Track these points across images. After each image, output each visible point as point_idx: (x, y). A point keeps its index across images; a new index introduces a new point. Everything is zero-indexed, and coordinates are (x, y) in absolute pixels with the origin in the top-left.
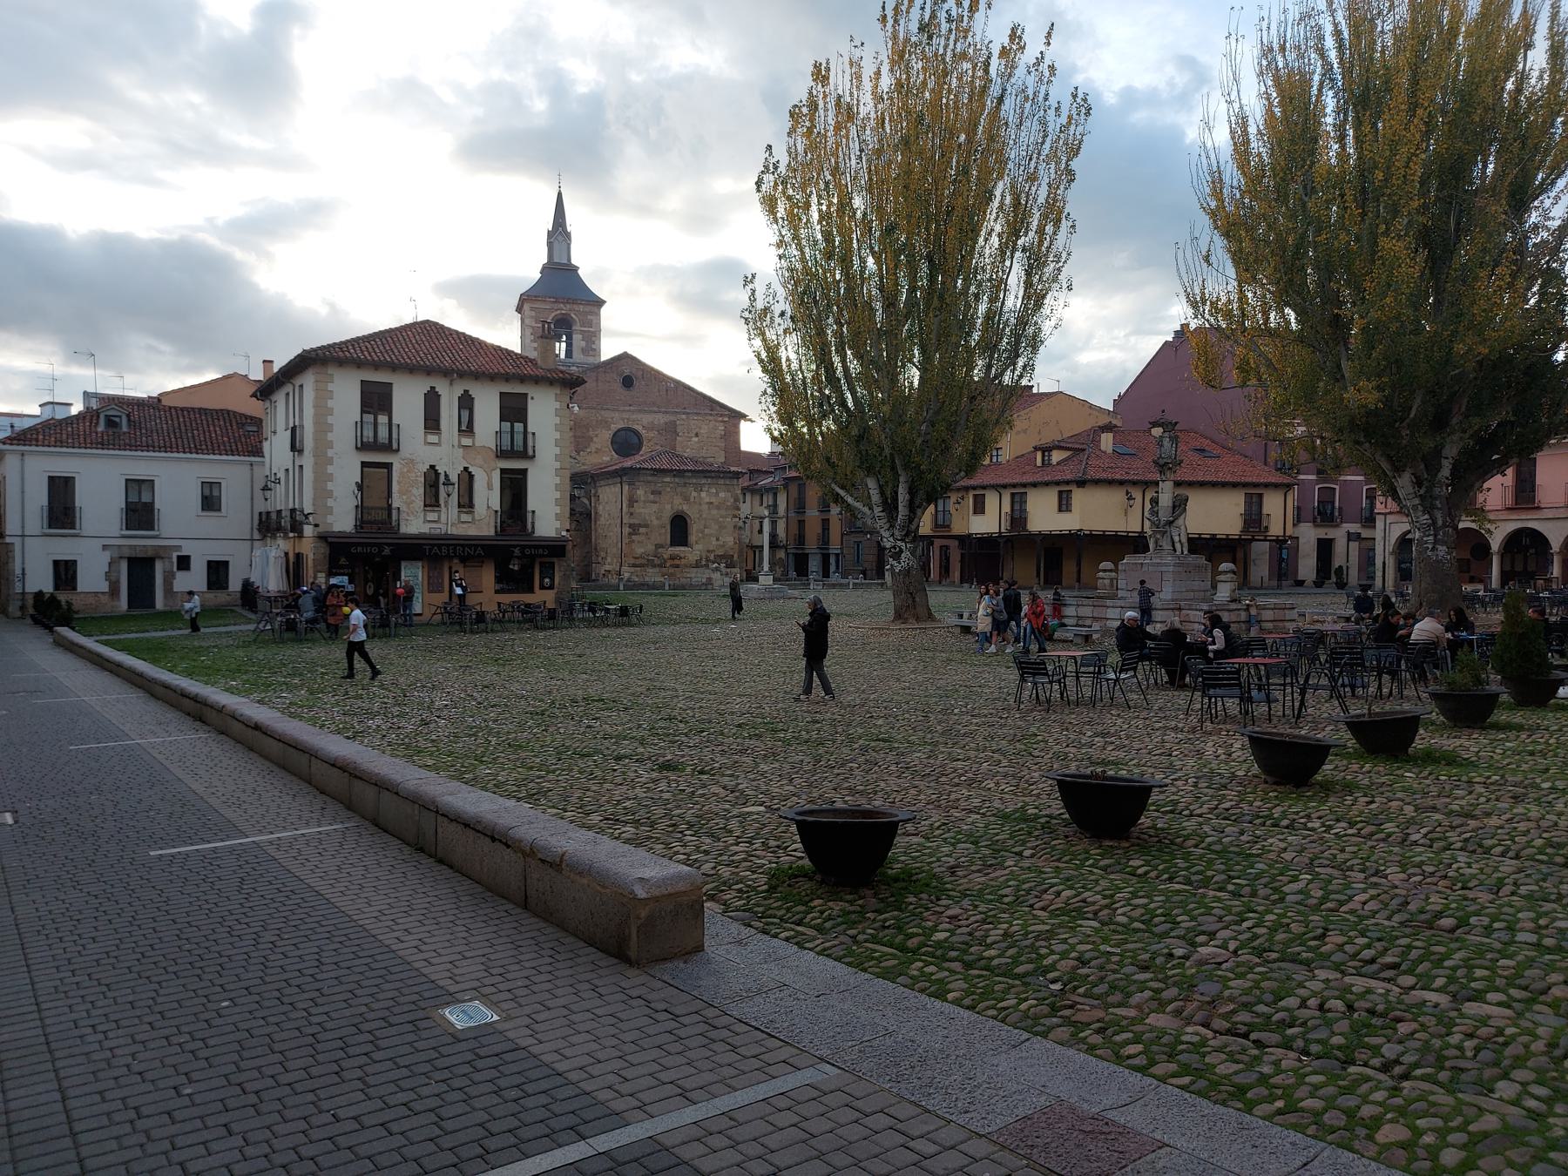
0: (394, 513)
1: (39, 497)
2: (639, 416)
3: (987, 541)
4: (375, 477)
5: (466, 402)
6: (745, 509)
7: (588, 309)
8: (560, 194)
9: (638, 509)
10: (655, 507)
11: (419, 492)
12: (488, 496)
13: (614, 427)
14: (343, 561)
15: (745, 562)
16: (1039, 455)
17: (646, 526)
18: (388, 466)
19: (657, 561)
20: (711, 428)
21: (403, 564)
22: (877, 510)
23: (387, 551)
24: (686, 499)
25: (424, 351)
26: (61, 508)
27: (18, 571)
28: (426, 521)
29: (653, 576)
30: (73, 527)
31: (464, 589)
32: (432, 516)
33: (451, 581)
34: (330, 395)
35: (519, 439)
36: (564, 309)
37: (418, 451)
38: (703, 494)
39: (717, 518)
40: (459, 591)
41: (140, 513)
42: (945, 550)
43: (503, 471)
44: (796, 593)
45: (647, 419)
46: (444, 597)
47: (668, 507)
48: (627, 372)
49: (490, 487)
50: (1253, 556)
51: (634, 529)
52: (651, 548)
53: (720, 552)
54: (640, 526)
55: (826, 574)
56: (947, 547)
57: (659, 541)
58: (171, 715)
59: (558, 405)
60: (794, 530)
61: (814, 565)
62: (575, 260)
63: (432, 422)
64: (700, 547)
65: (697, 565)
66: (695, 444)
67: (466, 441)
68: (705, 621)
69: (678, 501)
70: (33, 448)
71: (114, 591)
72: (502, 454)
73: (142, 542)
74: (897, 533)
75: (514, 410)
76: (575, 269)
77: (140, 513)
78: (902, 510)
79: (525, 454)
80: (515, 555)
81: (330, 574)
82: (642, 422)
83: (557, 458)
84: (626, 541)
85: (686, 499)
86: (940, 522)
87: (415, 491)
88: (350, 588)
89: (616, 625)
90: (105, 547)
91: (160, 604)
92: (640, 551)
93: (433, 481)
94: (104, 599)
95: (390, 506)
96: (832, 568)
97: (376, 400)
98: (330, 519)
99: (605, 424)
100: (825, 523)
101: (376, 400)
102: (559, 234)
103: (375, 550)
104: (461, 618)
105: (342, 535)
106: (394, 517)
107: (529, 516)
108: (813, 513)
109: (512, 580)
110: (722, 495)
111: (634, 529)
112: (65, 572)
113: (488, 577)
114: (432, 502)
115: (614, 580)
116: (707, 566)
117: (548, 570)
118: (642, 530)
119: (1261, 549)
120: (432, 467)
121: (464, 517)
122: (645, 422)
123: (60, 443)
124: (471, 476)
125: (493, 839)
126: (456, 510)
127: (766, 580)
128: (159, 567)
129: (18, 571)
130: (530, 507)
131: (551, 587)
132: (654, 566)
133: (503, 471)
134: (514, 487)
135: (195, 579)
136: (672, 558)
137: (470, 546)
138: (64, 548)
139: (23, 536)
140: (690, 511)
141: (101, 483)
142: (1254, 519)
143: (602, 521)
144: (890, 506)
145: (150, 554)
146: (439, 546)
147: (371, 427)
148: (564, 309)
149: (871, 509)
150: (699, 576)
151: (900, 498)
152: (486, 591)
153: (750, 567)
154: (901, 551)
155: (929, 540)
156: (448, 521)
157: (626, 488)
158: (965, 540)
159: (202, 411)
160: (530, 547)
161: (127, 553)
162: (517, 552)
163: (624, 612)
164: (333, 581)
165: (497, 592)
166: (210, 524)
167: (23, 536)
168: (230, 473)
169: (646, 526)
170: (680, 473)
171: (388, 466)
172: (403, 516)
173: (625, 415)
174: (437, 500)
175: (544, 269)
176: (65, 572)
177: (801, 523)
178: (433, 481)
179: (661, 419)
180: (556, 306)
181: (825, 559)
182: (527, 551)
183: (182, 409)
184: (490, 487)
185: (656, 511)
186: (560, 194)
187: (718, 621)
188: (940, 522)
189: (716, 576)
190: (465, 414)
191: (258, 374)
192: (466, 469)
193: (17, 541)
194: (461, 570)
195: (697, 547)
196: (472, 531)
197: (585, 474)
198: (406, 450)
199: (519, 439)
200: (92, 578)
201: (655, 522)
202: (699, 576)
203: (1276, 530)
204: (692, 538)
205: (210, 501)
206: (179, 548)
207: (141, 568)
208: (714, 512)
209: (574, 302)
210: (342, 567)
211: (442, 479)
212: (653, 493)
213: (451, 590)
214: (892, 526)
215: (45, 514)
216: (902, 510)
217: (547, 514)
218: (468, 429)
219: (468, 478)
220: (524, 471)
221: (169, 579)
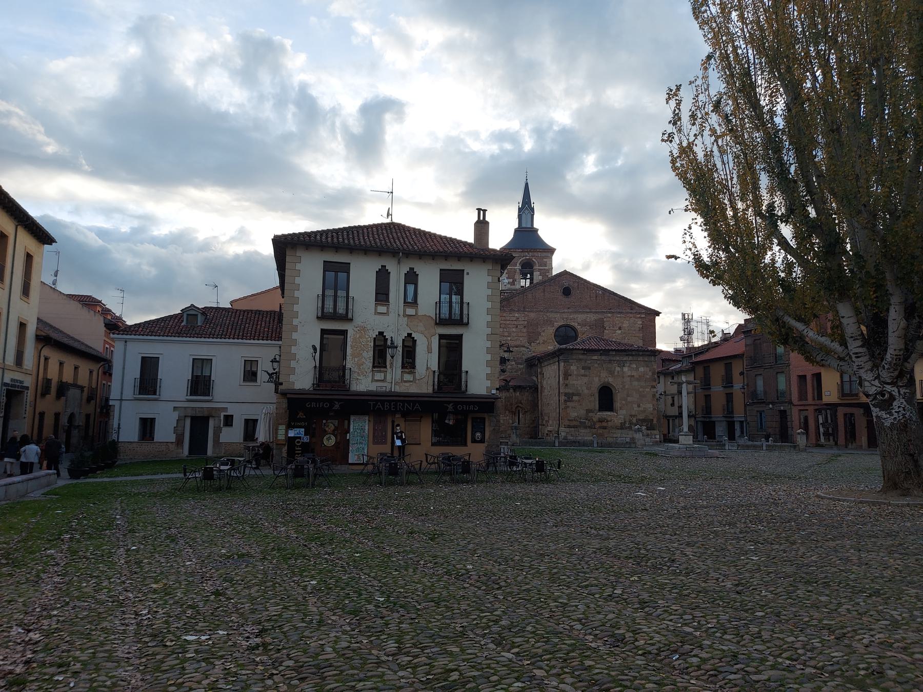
0: (347, 372)
1: (134, 371)
2: (575, 316)
4: (332, 342)
5: (411, 278)
6: (660, 388)
7: (544, 254)
8: (527, 185)
9: (572, 381)
10: (585, 380)
11: (368, 355)
12: (428, 358)
13: (557, 325)
14: (301, 415)
15: (665, 427)
17: (579, 395)
18: (344, 333)
19: (588, 423)
20: (630, 324)
21: (352, 418)
22: (854, 346)
23: (337, 406)
24: (611, 373)
25: (394, 244)
26: (148, 381)
27: (115, 426)
28: (373, 380)
29: (585, 435)
30: (155, 393)
31: (403, 441)
32: (380, 376)
33: (393, 433)
35: (456, 308)
36: (528, 256)
37: (368, 319)
38: (626, 369)
39: (635, 390)
40: (398, 443)
41: (200, 384)
42: (849, 418)
43: (441, 337)
44: (716, 452)
45: (580, 317)
46: (386, 449)
47: (596, 379)
48: (566, 285)
49: (430, 351)
51: (569, 397)
52: (582, 412)
53: (641, 417)
54: (573, 394)
55: (732, 437)
56: (852, 415)
59: (490, 279)
60: (702, 402)
61: (721, 430)
62: (535, 226)
63: (382, 295)
64: (624, 412)
65: (622, 427)
66: (620, 332)
67: (410, 311)
68: (628, 480)
69: (604, 374)
70: (133, 337)
71: (179, 441)
72: (441, 322)
73: (201, 404)
74: (885, 375)
75: (453, 282)
76: (536, 230)
77: (200, 384)
78: (894, 343)
79: (461, 322)
80: (451, 410)
81: (290, 427)
82: (578, 320)
83: (488, 324)
84: (562, 406)
85: (611, 373)
86: (847, 390)
87: (365, 354)
88: (306, 439)
89: (534, 481)
90: (175, 408)
91: (210, 452)
92: (574, 414)
93: (381, 348)
94: (172, 447)
95: (344, 367)
96: (738, 433)
97: (336, 273)
98: (292, 378)
99: (550, 322)
100: (729, 397)
101: (336, 273)
103: (326, 405)
104: (391, 471)
105: (301, 392)
106: (347, 377)
107: (463, 375)
108: (717, 389)
109: (449, 434)
110: (641, 369)
111: (569, 397)
112: (147, 426)
113: (425, 430)
115: (550, 439)
116: (630, 428)
117: (479, 425)
118: (575, 398)
120: (381, 333)
121: (407, 377)
122: (579, 320)
123: (152, 333)
124: (414, 341)
126: (399, 371)
127: (686, 440)
128: (211, 423)
129: (115, 426)
130: (464, 369)
131: (482, 441)
132: (586, 427)
133: (441, 337)
134: (452, 349)
135: (233, 435)
136: (601, 421)
137: (409, 402)
138: (147, 409)
139: (121, 400)
141: (176, 361)
143: (546, 392)
144: (875, 341)
145: (206, 414)
146: (383, 402)
147: (332, 299)
148: (528, 256)
149: (844, 343)
150: (624, 436)
151: (892, 326)
152: (422, 444)
153: (666, 432)
154: (892, 398)
155: (833, 407)
156: (393, 380)
157: (562, 364)
159: (259, 312)
160: (462, 403)
161: (190, 413)
162: (450, 407)
163: (540, 467)
164: (291, 434)
165: (433, 445)
166: (249, 391)
167: (121, 400)
168: (262, 353)
170: (606, 352)
171: (344, 333)
172: (355, 376)
173: (565, 316)
174: (385, 363)
175: (516, 231)
176: (147, 426)
177: (708, 397)
178: (381, 349)
179: (592, 317)
180: (522, 254)
181: (731, 426)
182: (460, 407)
183: (244, 311)
184: (430, 351)
185: (586, 381)
186: (527, 185)
187: (642, 480)
188: (847, 390)
189: (638, 436)
190: (411, 288)
192: (409, 335)
193: (117, 404)
194: (402, 424)
195: (621, 412)
196: (413, 389)
197: (534, 358)
198: (359, 319)
199: (456, 308)
200: (164, 433)
201: (586, 391)
202: (624, 436)
204: (617, 405)
205: (250, 375)
206: (225, 409)
207: (199, 423)
208: (636, 383)
209: (535, 250)
210: (301, 420)
211: (389, 343)
212: (583, 368)
213: (393, 442)
214: (875, 366)
215: (138, 384)
217: (479, 376)
220: (460, 337)
221: (218, 431)
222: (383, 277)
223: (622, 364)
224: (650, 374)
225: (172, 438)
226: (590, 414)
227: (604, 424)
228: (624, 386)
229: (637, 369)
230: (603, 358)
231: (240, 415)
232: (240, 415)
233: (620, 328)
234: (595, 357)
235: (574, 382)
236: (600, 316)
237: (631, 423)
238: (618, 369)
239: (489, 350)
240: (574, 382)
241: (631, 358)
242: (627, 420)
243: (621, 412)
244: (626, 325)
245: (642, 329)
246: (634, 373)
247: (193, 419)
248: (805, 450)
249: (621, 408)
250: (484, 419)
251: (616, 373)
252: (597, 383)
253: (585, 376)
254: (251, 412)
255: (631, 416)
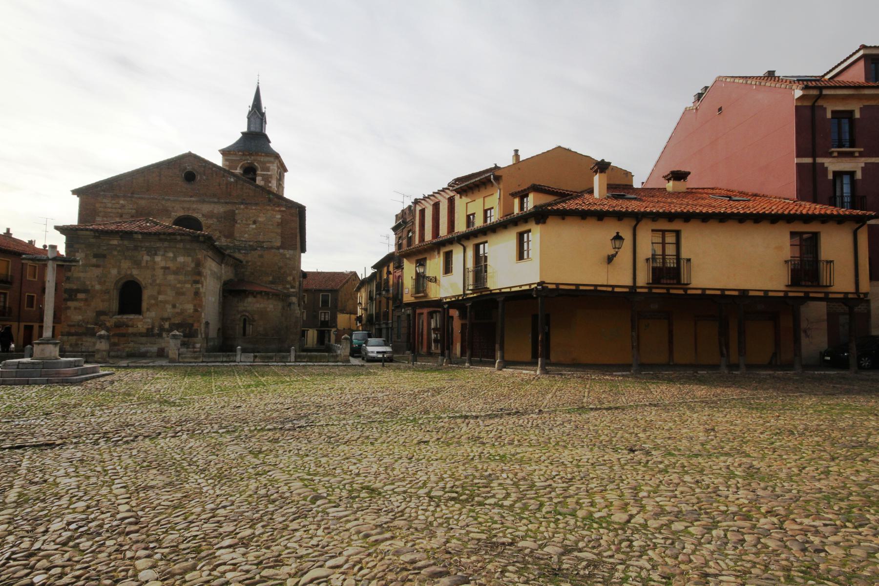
7: (267, 159)
10: (97, 272)
16: (517, 201)
17: (86, 291)
24: (137, 264)
38: (158, 259)
45: (206, 208)
50: (804, 325)
52: (91, 314)
53: (177, 321)
57: (102, 306)
58: (617, 377)
64: (153, 314)
102: (257, 113)
110: (181, 259)
118: (81, 296)
119: (815, 311)
142: (807, 269)
169: (86, 291)
179: (220, 209)
180: (244, 158)
201: (98, 287)
203: (841, 281)
208: (171, 278)
212: (96, 256)
223: (153, 252)
224: (193, 265)
226: (102, 318)
227: (123, 330)
228: (155, 281)
229: (175, 258)
230: (126, 243)
233: (255, 222)
234: (115, 242)
235: (82, 275)
236: (229, 207)
237: (162, 329)
238: (146, 258)
240: (82, 275)
241: (166, 244)
242: (157, 324)
243: (148, 314)
246: (170, 264)
249: (148, 310)
250: (380, 337)
251: (144, 264)
253: (98, 266)
255: (163, 319)
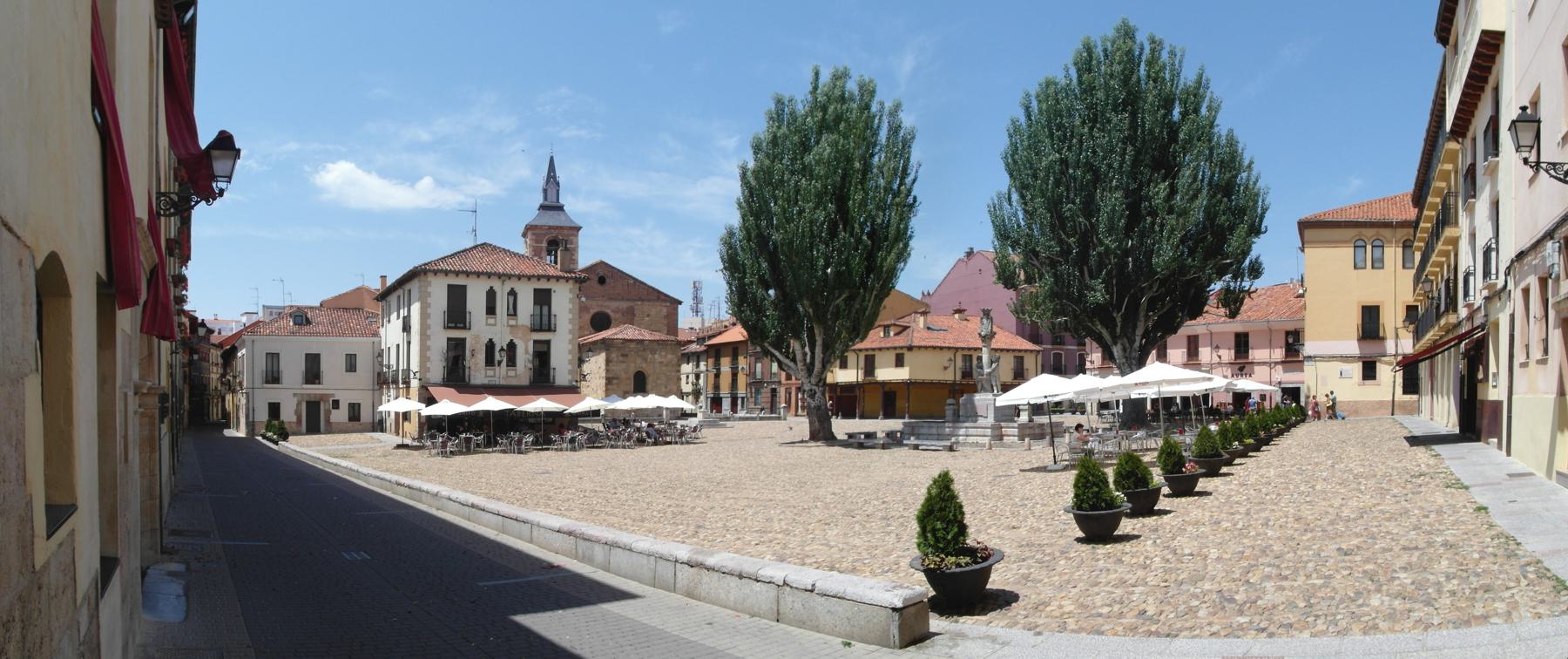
1: (261, 364)
3: (849, 388)
8: (552, 160)
11: (481, 357)
13: (593, 312)
24: (645, 360)
32: (490, 373)
34: (429, 295)
43: (535, 342)
45: (614, 304)
61: (726, 404)
63: (491, 310)
67: (512, 322)
69: (639, 361)
71: (299, 421)
72: (534, 330)
73: (313, 390)
75: (543, 298)
78: (818, 365)
79: (550, 328)
85: (645, 360)
114: (490, 361)
125: (741, 576)
133: (535, 342)
140: (644, 367)
158: (835, 386)
179: (624, 305)
186: (552, 160)
191: (376, 285)
199: (545, 319)
216: (818, 365)
218: (513, 312)
219: (512, 346)
220: (548, 343)
221: (328, 413)
222: (491, 295)
225: (294, 419)
231: (345, 399)
232: (345, 399)
239: (570, 352)
244: (653, 312)
245: (667, 317)
247: (308, 403)
248: (884, 447)
252: (632, 370)
254: (354, 397)
